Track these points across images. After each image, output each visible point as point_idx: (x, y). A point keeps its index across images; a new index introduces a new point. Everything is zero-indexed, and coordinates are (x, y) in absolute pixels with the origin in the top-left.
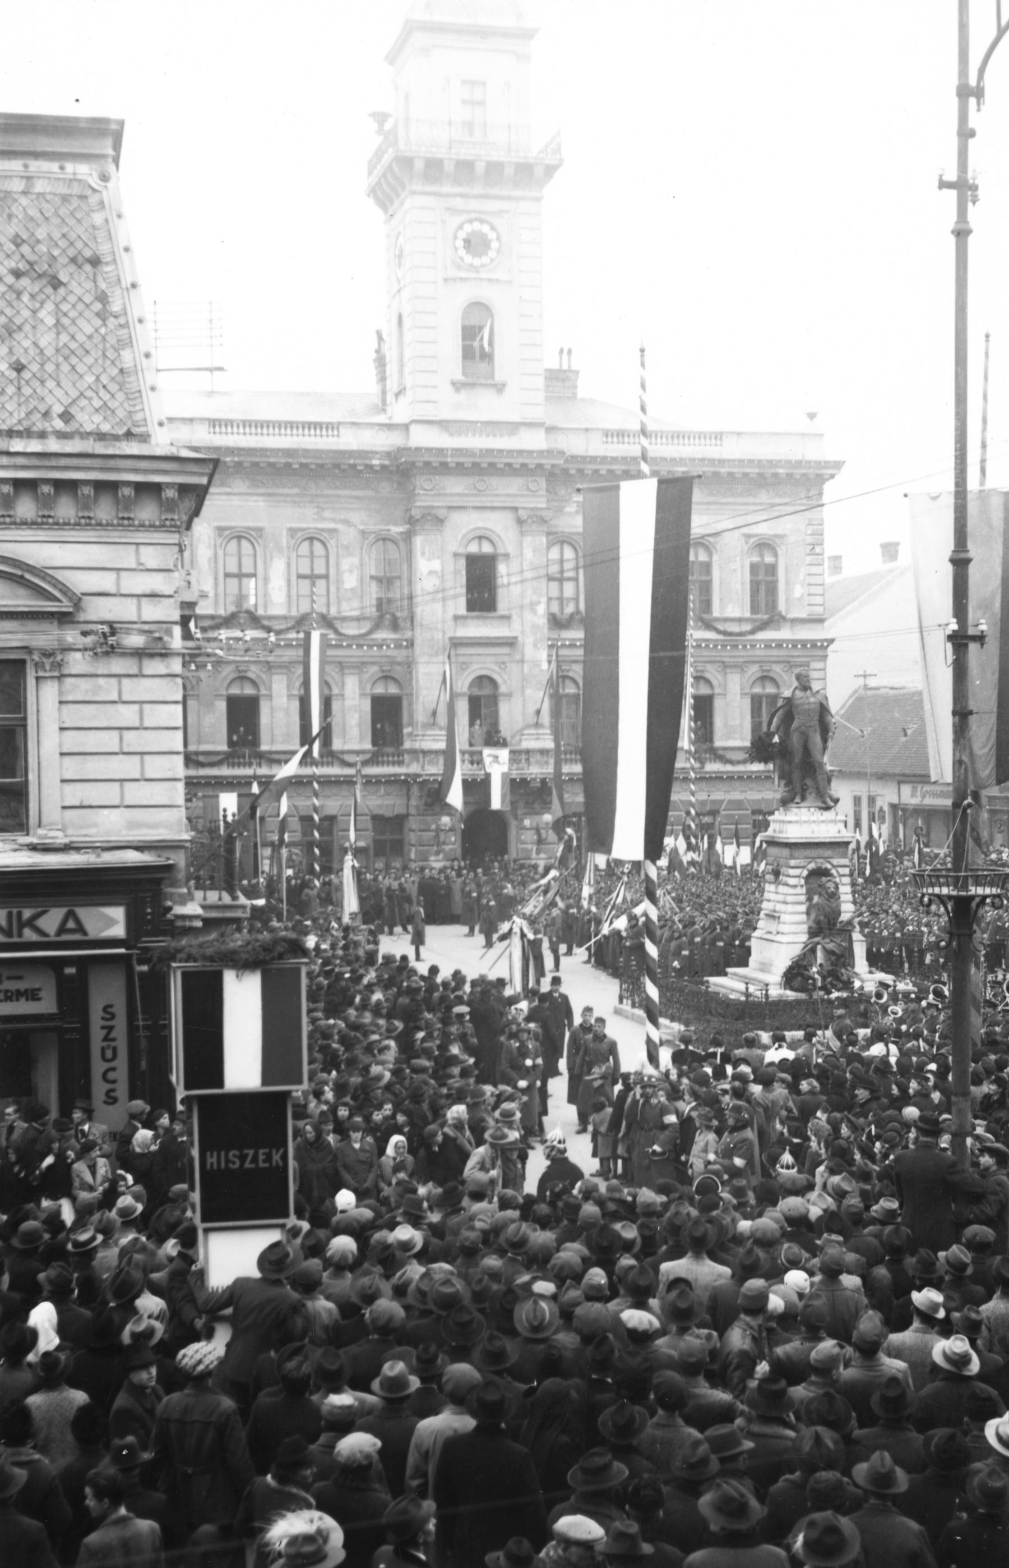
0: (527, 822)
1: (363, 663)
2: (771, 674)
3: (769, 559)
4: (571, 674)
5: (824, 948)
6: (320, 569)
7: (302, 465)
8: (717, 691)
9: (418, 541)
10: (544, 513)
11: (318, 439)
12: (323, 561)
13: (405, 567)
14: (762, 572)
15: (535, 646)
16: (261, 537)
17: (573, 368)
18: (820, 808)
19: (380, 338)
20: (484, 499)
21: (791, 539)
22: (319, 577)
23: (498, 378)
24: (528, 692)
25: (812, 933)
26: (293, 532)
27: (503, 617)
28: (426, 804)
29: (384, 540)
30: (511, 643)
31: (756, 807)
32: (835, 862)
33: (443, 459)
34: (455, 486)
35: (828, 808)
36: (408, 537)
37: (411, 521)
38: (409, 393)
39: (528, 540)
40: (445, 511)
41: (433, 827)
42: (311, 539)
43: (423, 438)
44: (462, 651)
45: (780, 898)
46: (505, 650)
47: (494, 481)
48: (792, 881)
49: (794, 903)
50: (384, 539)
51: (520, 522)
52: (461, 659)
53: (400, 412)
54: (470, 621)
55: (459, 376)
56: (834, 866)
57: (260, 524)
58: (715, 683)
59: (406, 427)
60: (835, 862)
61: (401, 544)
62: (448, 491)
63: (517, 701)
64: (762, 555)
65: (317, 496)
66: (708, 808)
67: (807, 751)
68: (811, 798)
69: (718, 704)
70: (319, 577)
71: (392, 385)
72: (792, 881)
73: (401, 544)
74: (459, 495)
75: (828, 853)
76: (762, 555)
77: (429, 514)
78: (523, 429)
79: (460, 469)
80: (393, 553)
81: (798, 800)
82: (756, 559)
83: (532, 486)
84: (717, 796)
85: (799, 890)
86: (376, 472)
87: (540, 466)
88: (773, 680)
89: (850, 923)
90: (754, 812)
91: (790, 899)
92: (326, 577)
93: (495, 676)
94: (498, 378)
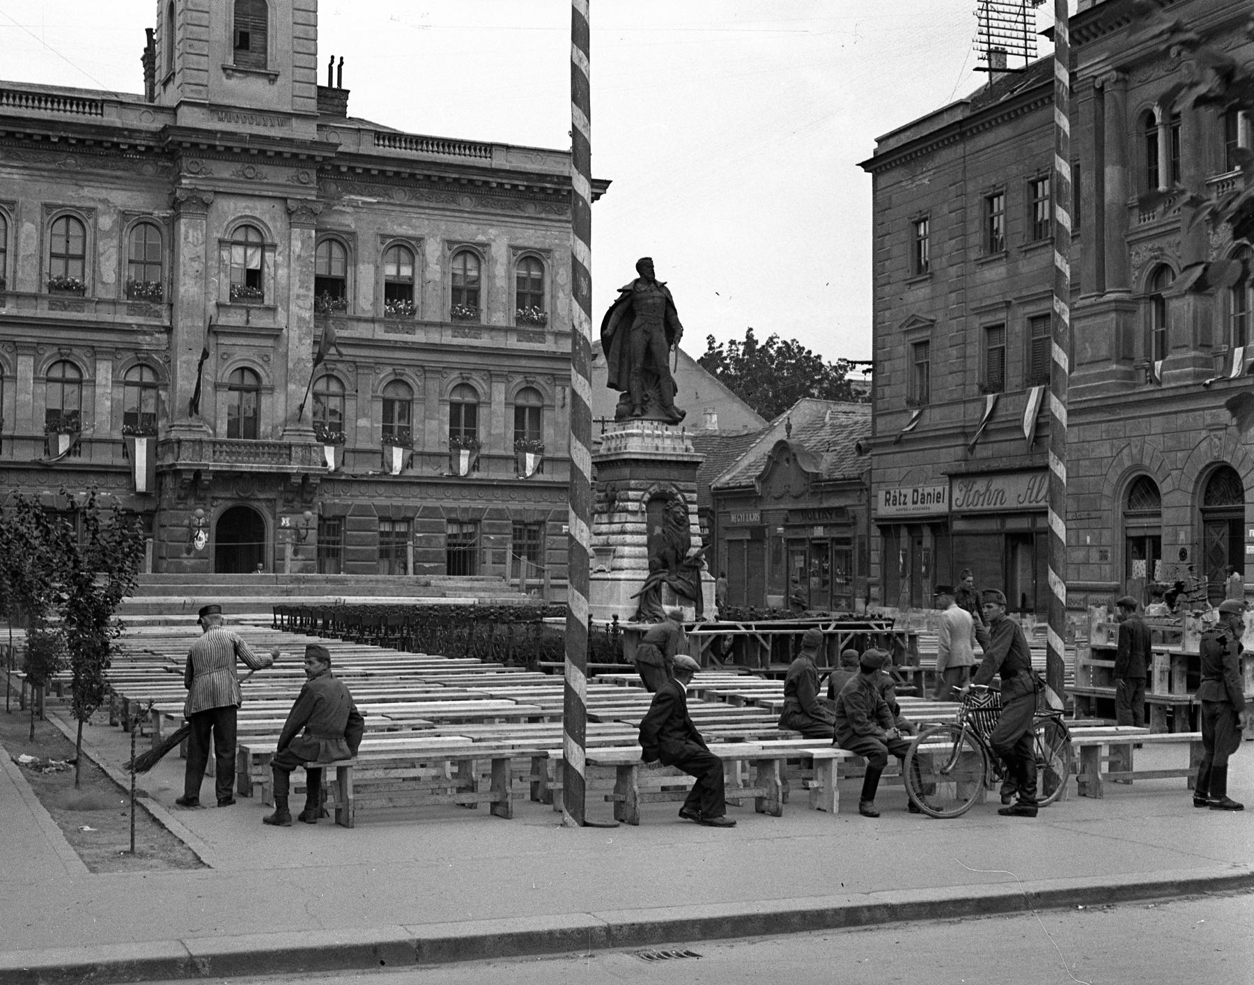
0: (286, 521)
1: (117, 349)
2: (534, 386)
3: (535, 273)
4: (335, 373)
5: (671, 586)
6: (75, 249)
7: (61, 138)
8: (483, 399)
9: (183, 224)
10: (314, 206)
11: (80, 115)
12: (80, 241)
13: (167, 252)
14: (529, 283)
15: (300, 339)
16: (12, 210)
17: (343, 87)
18: (664, 422)
19: (150, 41)
20: (253, 186)
21: (557, 255)
22: (74, 257)
23: (271, 68)
24: (292, 387)
25: (653, 569)
26: (48, 207)
27: (268, 309)
28: (179, 498)
29: (146, 223)
30: (276, 335)
31: (518, 518)
32: (681, 485)
33: (212, 142)
34: (224, 171)
35: (675, 422)
36: (172, 222)
37: (175, 204)
38: (178, 79)
39: (296, 232)
40: (211, 196)
41: (186, 522)
42: (68, 217)
43: (188, 118)
44: (222, 340)
45: (615, 527)
46: (270, 342)
47: (265, 169)
48: (632, 506)
49: (632, 533)
50: (145, 222)
51: (290, 213)
52: (222, 349)
53: (169, 97)
54: (232, 311)
55: (230, 62)
56: (681, 491)
57: (13, 198)
58: (480, 390)
59: (174, 111)
60: (681, 485)
61: (164, 230)
62: (216, 176)
63: (280, 397)
64: (529, 270)
65: (78, 173)
66: (470, 516)
67: (649, 353)
68: (653, 412)
69: (482, 412)
70: (74, 257)
71: (160, 75)
72: (632, 506)
73: (164, 230)
74: (226, 180)
75: (674, 473)
76: (529, 270)
77: (196, 198)
78: (294, 121)
79: (228, 154)
80: (154, 239)
81: (638, 412)
82: (523, 273)
83: (304, 178)
84: (479, 504)
85: (639, 518)
86: (140, 153)
87: (311, 157)
88: (537, 392)
89: (697, 558)
90: (514, 522)
91: (629, 527)
92: (82, 257)
93: (258, 369)
94: (271, 68)
